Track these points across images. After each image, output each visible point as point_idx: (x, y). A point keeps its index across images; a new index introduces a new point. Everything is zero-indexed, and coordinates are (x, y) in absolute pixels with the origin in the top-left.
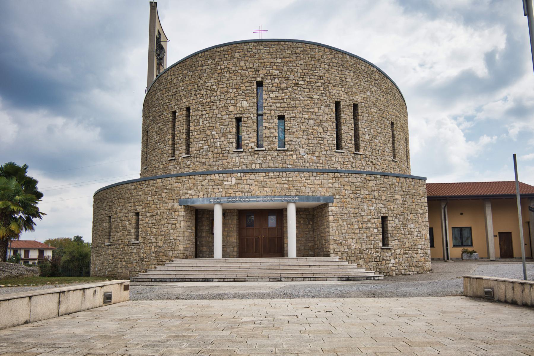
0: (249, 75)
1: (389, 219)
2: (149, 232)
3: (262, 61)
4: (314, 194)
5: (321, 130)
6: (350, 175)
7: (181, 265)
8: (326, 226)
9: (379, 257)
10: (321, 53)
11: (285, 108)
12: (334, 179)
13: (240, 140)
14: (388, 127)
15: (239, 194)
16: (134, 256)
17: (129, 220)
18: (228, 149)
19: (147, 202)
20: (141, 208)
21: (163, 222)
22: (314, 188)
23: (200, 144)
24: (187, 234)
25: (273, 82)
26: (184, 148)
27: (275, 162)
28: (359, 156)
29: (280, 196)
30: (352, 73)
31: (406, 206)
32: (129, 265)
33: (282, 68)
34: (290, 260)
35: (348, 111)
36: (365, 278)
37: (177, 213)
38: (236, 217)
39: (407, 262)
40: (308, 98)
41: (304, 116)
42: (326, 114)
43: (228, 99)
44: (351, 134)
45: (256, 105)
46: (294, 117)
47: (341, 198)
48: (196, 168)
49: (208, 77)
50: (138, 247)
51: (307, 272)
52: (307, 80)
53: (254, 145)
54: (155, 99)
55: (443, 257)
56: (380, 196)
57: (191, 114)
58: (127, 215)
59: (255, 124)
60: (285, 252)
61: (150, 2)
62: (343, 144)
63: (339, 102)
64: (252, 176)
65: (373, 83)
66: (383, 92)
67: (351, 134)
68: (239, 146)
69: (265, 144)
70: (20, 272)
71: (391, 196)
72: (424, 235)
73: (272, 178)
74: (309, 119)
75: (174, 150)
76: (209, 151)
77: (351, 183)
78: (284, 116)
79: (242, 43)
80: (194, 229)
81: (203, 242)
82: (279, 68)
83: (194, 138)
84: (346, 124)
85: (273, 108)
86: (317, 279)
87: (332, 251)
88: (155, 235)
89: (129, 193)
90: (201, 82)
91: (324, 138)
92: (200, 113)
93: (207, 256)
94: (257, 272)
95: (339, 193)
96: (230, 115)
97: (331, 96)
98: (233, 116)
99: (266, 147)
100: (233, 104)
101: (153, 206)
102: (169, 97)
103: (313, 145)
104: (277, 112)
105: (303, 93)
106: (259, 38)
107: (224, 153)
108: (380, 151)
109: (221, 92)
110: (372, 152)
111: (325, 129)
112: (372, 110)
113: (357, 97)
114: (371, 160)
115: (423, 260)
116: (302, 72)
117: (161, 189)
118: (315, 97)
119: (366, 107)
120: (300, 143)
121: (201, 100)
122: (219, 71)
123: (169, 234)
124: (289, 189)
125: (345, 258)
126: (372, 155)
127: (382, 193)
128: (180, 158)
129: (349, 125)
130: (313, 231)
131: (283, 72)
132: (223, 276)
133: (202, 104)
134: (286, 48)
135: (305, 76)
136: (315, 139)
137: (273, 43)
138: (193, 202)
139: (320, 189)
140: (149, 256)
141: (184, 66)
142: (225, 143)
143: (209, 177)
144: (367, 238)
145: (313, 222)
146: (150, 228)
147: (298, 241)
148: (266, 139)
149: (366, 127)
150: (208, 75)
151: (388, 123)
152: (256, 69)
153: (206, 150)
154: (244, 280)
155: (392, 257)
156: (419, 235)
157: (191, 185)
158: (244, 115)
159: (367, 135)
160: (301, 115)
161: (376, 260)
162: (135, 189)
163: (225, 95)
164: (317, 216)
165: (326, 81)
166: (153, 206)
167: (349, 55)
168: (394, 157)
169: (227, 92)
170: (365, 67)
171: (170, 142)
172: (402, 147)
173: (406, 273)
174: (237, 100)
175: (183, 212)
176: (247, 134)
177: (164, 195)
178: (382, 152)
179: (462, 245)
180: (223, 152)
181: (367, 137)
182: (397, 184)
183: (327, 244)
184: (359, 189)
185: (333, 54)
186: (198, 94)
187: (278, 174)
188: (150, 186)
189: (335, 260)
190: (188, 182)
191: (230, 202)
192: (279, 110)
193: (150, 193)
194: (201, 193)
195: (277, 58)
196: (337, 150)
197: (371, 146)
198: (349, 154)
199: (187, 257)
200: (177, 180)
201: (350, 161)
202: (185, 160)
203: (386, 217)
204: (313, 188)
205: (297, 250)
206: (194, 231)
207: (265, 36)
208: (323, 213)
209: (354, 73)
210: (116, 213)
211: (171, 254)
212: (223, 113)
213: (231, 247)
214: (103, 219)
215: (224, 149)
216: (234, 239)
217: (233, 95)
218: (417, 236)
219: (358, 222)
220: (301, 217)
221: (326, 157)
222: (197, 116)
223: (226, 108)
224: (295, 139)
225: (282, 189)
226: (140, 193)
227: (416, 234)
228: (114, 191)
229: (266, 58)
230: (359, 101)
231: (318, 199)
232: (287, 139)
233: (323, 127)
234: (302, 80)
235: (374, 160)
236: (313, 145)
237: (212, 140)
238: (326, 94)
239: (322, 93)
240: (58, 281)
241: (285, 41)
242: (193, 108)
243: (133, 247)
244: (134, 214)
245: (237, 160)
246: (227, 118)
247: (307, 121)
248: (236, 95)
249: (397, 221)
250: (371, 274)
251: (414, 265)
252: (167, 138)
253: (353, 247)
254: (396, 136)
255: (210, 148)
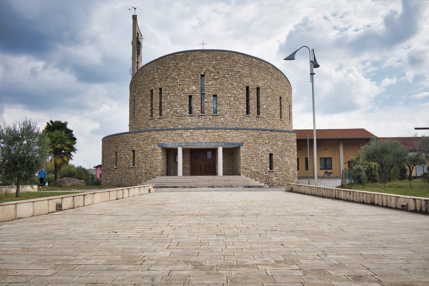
0: (197, 71)
1: (274, 155)
2: (141, 161)
3: (204, 62)
4: (233, 141)
5: (238, 103)
6: (252, 131)
7: (160, 179)
8: (239, 159)
9: (268, 176)
10: (238, 58)
11: (217, 91)
12: (244, 133)
13: (191, 109)
14: (278, 100)
15: (191, 141)
16: (133, 174)
17: (128, 155)
18: (184, 114)
19: (140, 145)
20: (136, 148)
21: (149, 156)
22: (233, 138)
23: (168, 110)
24: (162, 163)
25: (210, 75)
26: (158, 112)
27: (211, 122)
28: (260, 118)
29: (214, 143)
30: (256, 69)
31: (284, 148)
32: (129, 180)
33: (215, 67)
34: (219, 177)
35: (254, 92)
36: (258, 187)
37: (157, 151)
38: (189, 153)
39: (283, 178)
40: (230, 85)
41: (228, 95)
42: (241, 94)
43: (185, 84)
44: (255, 105)
45: (200, 88)
46: (222, 96)
47: (247, 144)
48: (166, 124)
49: (172, 71)
50: (135, 169)
51: (228, 183)
52: (230, 74)
53: (199, 112)
54: (139, 81)
55: (339, 176)
56: (269, 142)
57: (162, 92)
58: (127, 151)
59: (200, 100)
60: (216, 173)
61: (133, 15)
62: (251, 111)
63: (249, 87)
64: (199, 132)
65: (269, 74)
66: (275, 79)
67: (255, 105)
68: (190, 112)
69: (206, 111)
70: (77, 183)
71: (275, 142)
72: (293, 164)
73: (210, 133)
74: (231, 97)
75: (152, 113)
76: (173, 115)
77: (253, 136)
78: (217, 95)
79: (192, 51)
80: (166, 159)
81: (171, 167)
82: (214, 67)
83: (164, 107)
84: (252, 100)
85: (210, 90)
86: (233, 187)
87: (242, 172)
88: (145, 163)
89: (128, 139)
90: (168, 74)
91: (239, 108)
92: (168, 92)
93: (173, 175)
94: (202, 183)
95: (246, 141)
96: (186, 94)
97: (244, 83)
98: (187, 95)
99: (206, 113)
100: (187, 88)
101: (143, 147)
102: (149, 81)
103: (233, 112)
104: (212, 93)
105: (228, 82)
106: (202, 49)
107: (182, 116)
108: (272, 114)
109: (180, 80)
110: (267, 116)
111: (240, 103)
112: (268, 91)
113: (259, 83)
114: (266, 120)
115: (293, 178)
116: (227, 69)
117: (148, 137)
118: (235, 84)
119: (264, 89)
120: (225, 111)
121: (168, 84)
122: (179, 68)
123: (153, 163)
124: (219, 138)
125: (249, 176)
126: (267, 117)
127: (270, 141)
128: (156, 118)
129: (254, 100)
130: (232, 161)
131: (216, 70)
132: (184, 185)
133: (169, 87)
134: (218, 55)
135: (229, 72)
136: (234, 108)
137: (211, 52)
138: (166, 145)
139: (236, 139)
140: (141, 175)
141: (158, 63)
142: (183, 110)
143: (175, 132)
144: (261, 165)
145: (232, 156)
146: (141, 159)
147: (224, 166)
148: (206, 108)
149: (264, 101)
150: (172, 70)
151: (278, 98)
152: (200, 67)
153: (172, 114)
154: (195, 187)
155: (274, 176)
156: (291, 164)
157: (165, 136)
158: (194, 94)
159: (265, 105)
160: (226, 95)
161: (266, 177)
162: (132, 137)
163: (182, 82)
164: (234, 153)
165: (241, 75)
166: (143, 147)
167: (255, 58)
168: (281, 118)
169: (184, 81)
170: (264, 65)
171: (150, 108)
172: (286, 111)
173: (282, 184)
174: (189, 85)
175: (160, 151)
176: (195, 106)
177: (149, 141)
178: (274, 115)
179: (326, 169)
180: (181, 116)
181: (265, 107)
182: (279, 135)
183: (239, 168)
184: (257, 138)
185: (245, 58)
186: (167, 81)
187: (213, 130)
188: (141, 136)
189: (243, 177)
190: (163, 134)
191: (186, 145)
192: (214, 92)
193: (141, 140)
194: (171, 141)
195: (213, 61)
196: (247, 115)
197: (267, 112)
198: (254, 117)
199: (163, 175)
200: (157, 133)
201: (254, 121)
202: (159, 119)
203: (272, 154)
204: (232, 138)
205: (223, 172)
206: (166, 161)
207: (206, 47)
208: (238, 152)
209: (258, 69)
210: (120, 150)
211: (154, 174)
212: (181, 93)
213: (186, 169)
214: (112, 153)
215: (182, 114)
216: (188, 166)
217: (187, 82)
218: (290, 164)
219: (256, 157)
220: (226, 153)
221: (240, 119)
222: (166, 94)
223: (183, 90)
224: (223, 109)
225: (215, 139)
226: (135, 139)
227: (289, 163)
228: (119, 137)
229: (207, 61)
230: (260, 85)
231: (235, 144)
232: (218, 109)
233: (239, 101)
234: (227, 74)
235: (268, 120)
236: (233, 112)
237: (175, 108)
238: (241, 82)
239: (238, 82)
240: (98, 187)
241: (217, 51)
242: (163, 89)
243: (131, 170)
244: (132, 151)
245: (190, 120)
246: (184, 96)
247: (229, 98)
248: (189, 82)
249: (278, 156)
250: (263, 184)
251: (287, 180)
252: (148, 105)
253: (253, 170)
254: (282, 105)
255: (174, 113)
